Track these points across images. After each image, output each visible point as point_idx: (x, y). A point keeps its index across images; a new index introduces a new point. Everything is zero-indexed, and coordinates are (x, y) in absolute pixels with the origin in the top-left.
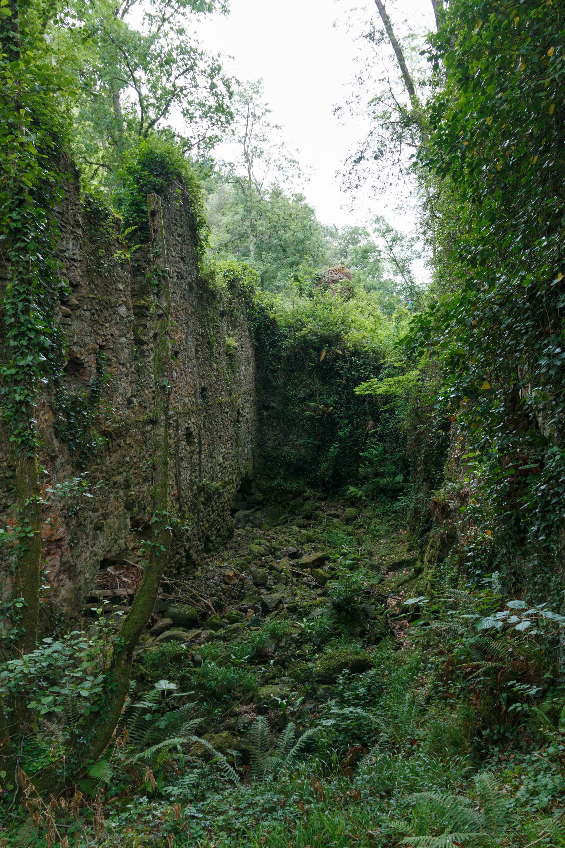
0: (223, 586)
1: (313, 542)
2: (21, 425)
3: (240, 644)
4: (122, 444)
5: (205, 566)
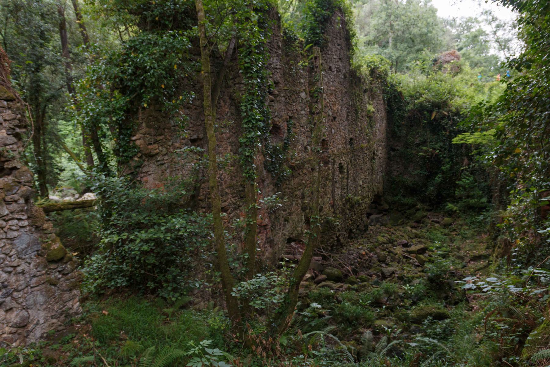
0: (359, 260)
1: (419, 238)
2: (248, 168)
3: (365, 294)
4: (301, 173)
5: (348, 247)
